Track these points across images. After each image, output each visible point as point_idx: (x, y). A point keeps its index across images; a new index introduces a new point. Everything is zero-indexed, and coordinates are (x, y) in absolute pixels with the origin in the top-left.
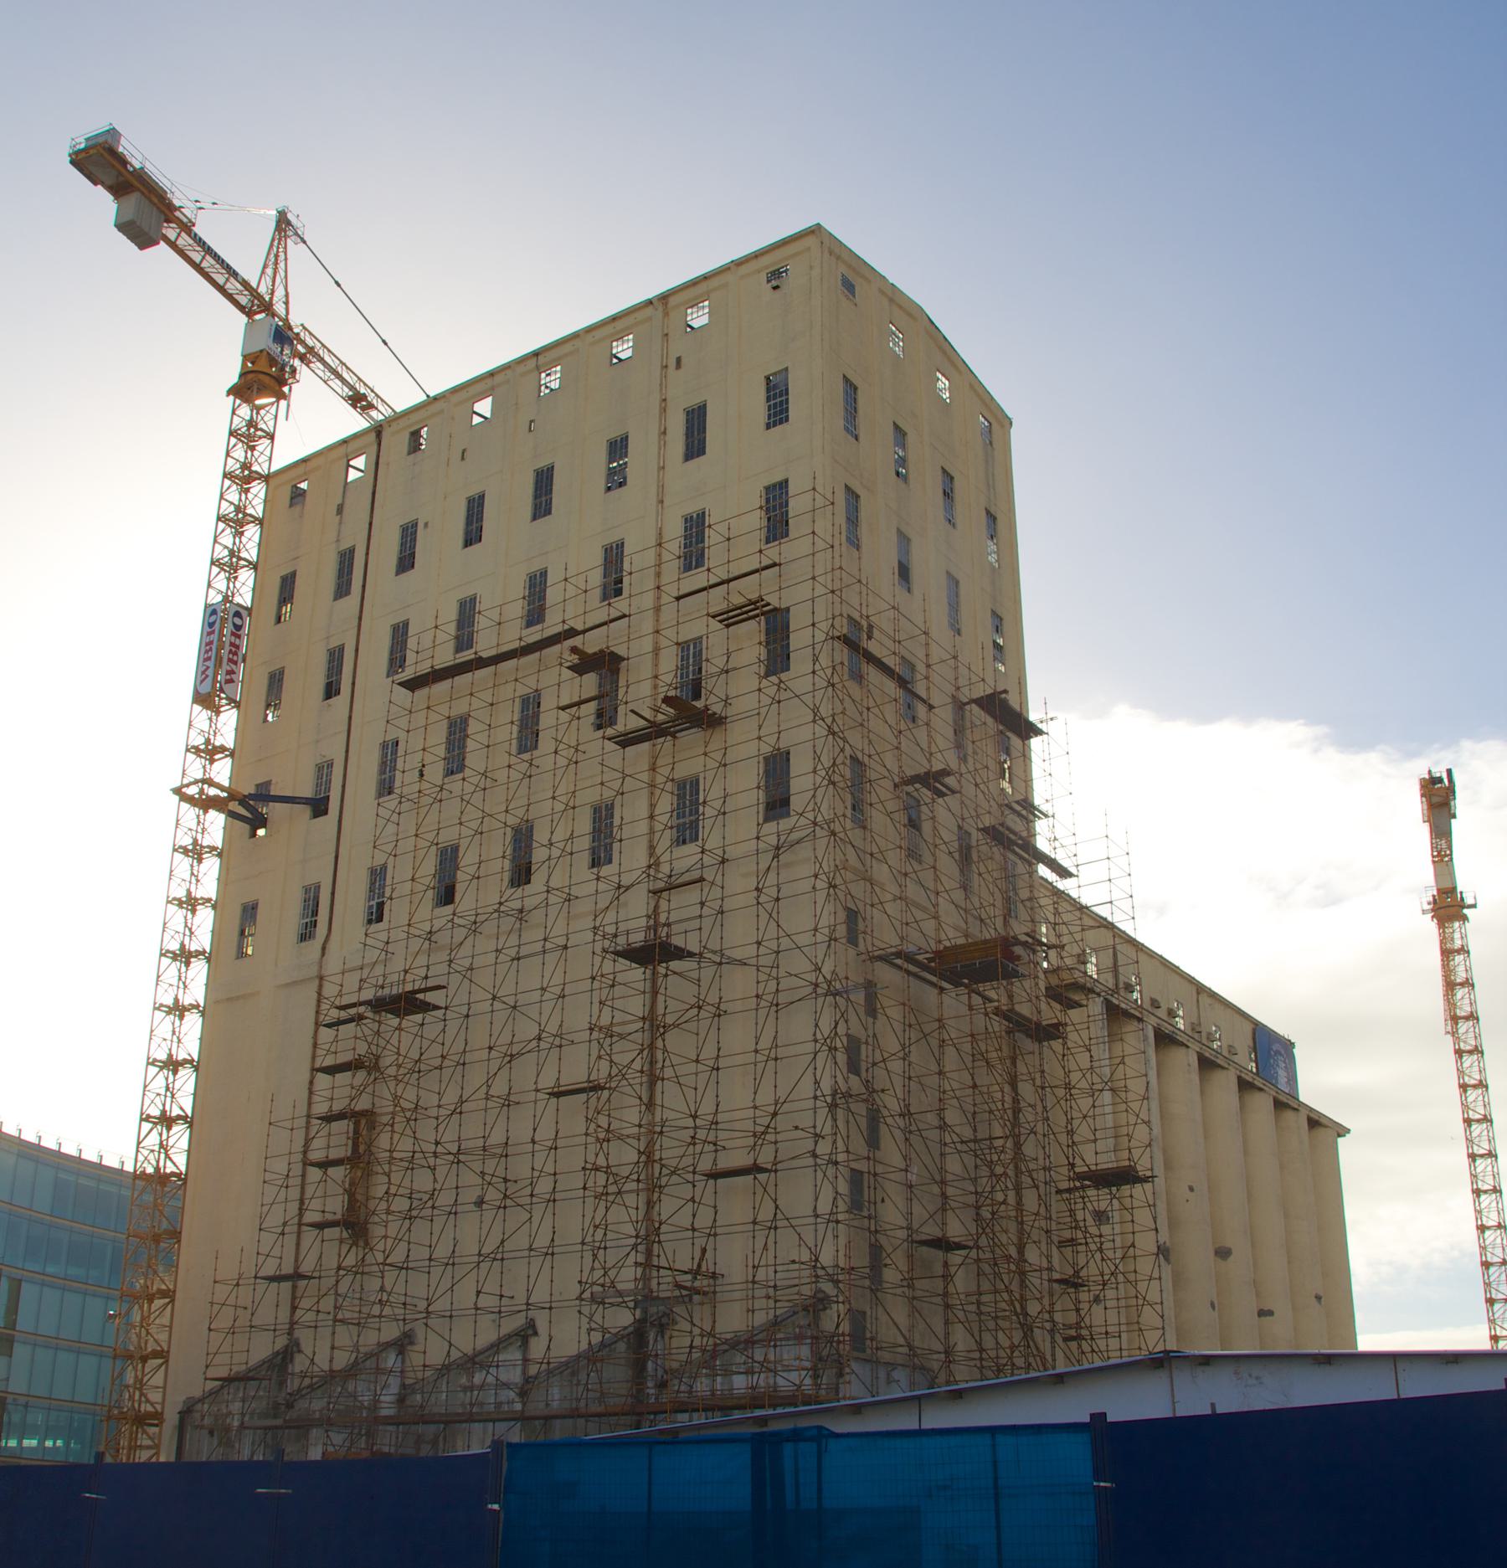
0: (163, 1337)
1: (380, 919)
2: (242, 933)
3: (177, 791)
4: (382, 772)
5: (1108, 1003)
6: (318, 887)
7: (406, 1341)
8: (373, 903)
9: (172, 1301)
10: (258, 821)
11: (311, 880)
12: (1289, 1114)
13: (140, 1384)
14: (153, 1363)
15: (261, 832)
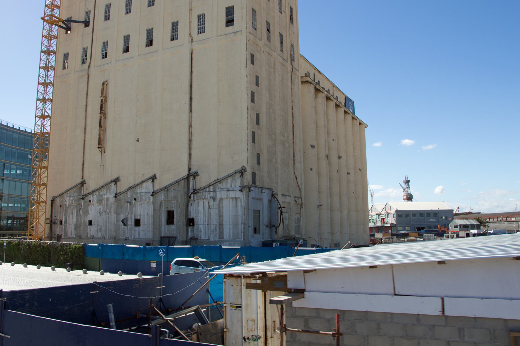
0: (45, 180)
1: (106, 57)
2: (64, 62)
3: (43, 18)
4: (106, 13)
5: (315, 87)
6: (87, 48)
7: (243, 171)
8: (104, 52)
9: (48, 169)
10: (68, 29)
11: (85, 46)
12: (355, 121)
13: (39, 193)
14: (42, 187)
15: (69, 32)
